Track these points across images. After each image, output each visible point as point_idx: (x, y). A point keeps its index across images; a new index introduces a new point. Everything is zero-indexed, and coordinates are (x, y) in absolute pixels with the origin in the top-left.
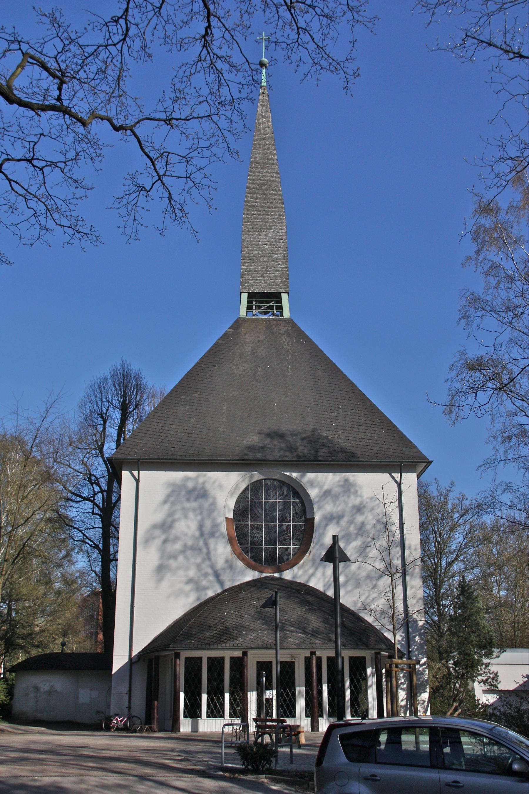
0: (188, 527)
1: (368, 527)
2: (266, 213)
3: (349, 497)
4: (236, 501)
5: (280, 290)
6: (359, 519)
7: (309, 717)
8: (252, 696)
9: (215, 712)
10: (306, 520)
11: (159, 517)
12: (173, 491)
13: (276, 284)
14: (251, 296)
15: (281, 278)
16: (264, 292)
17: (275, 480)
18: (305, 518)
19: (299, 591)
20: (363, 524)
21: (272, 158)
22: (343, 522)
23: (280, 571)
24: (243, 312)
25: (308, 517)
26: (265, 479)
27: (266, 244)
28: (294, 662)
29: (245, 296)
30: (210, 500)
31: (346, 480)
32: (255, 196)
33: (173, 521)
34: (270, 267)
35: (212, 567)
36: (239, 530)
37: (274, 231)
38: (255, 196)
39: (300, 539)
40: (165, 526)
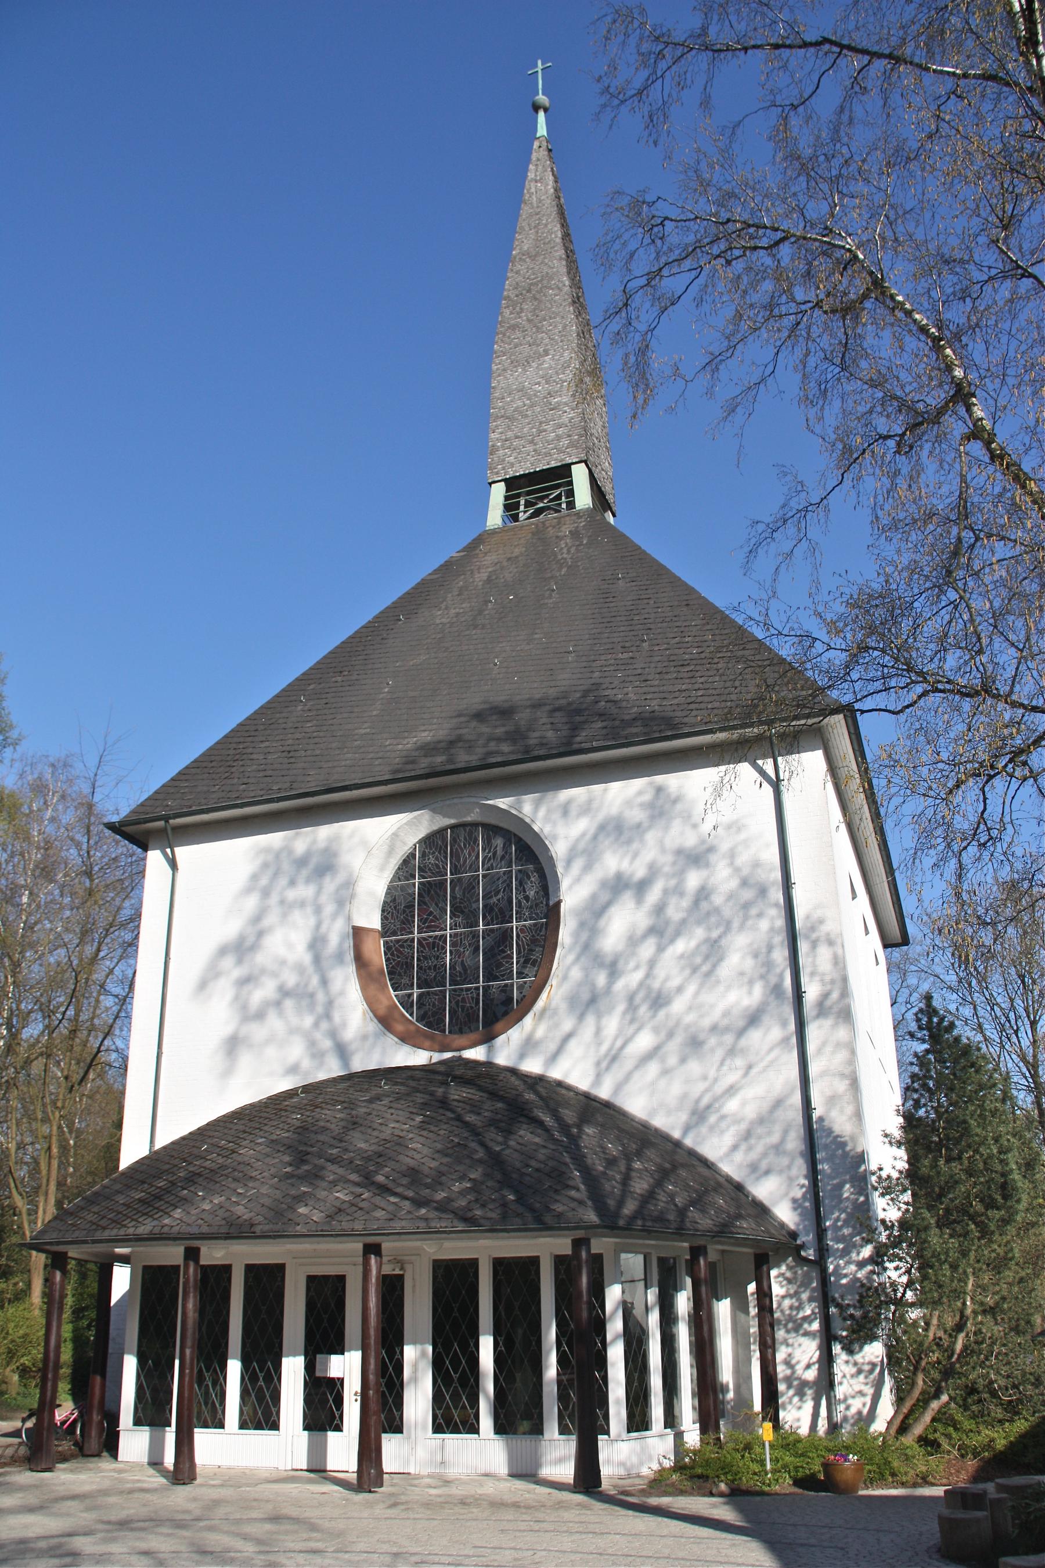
0: (290, 946)
1: (718, 900)
2: (539, 330)
3: (667, 828)
5: (568, 461)
6: (693, 880)
7: (570, 1433)
8: (293, 1370)
9: (262, 1415)
11: (231, 929)
12: (265, 865)
13: (560, 451)
14: (511, 483)
15: (569, 436)
16: (535, 472)
20: (703, 893)
21: (552, 239)
22: (654, 895)
23: (488, 1038)
24: (495, 517)
26: (453, 827)
27: (539, 383)
28: (401, 1277)
29: (498, 492)
30: (341, 878)
31: (659, 790)
32: (518, 309)
33: (260, 934)
34: (547, 423)
35: (333, 1034)
37: (554, 356)
38: (518, 309)
40: (241, 948)
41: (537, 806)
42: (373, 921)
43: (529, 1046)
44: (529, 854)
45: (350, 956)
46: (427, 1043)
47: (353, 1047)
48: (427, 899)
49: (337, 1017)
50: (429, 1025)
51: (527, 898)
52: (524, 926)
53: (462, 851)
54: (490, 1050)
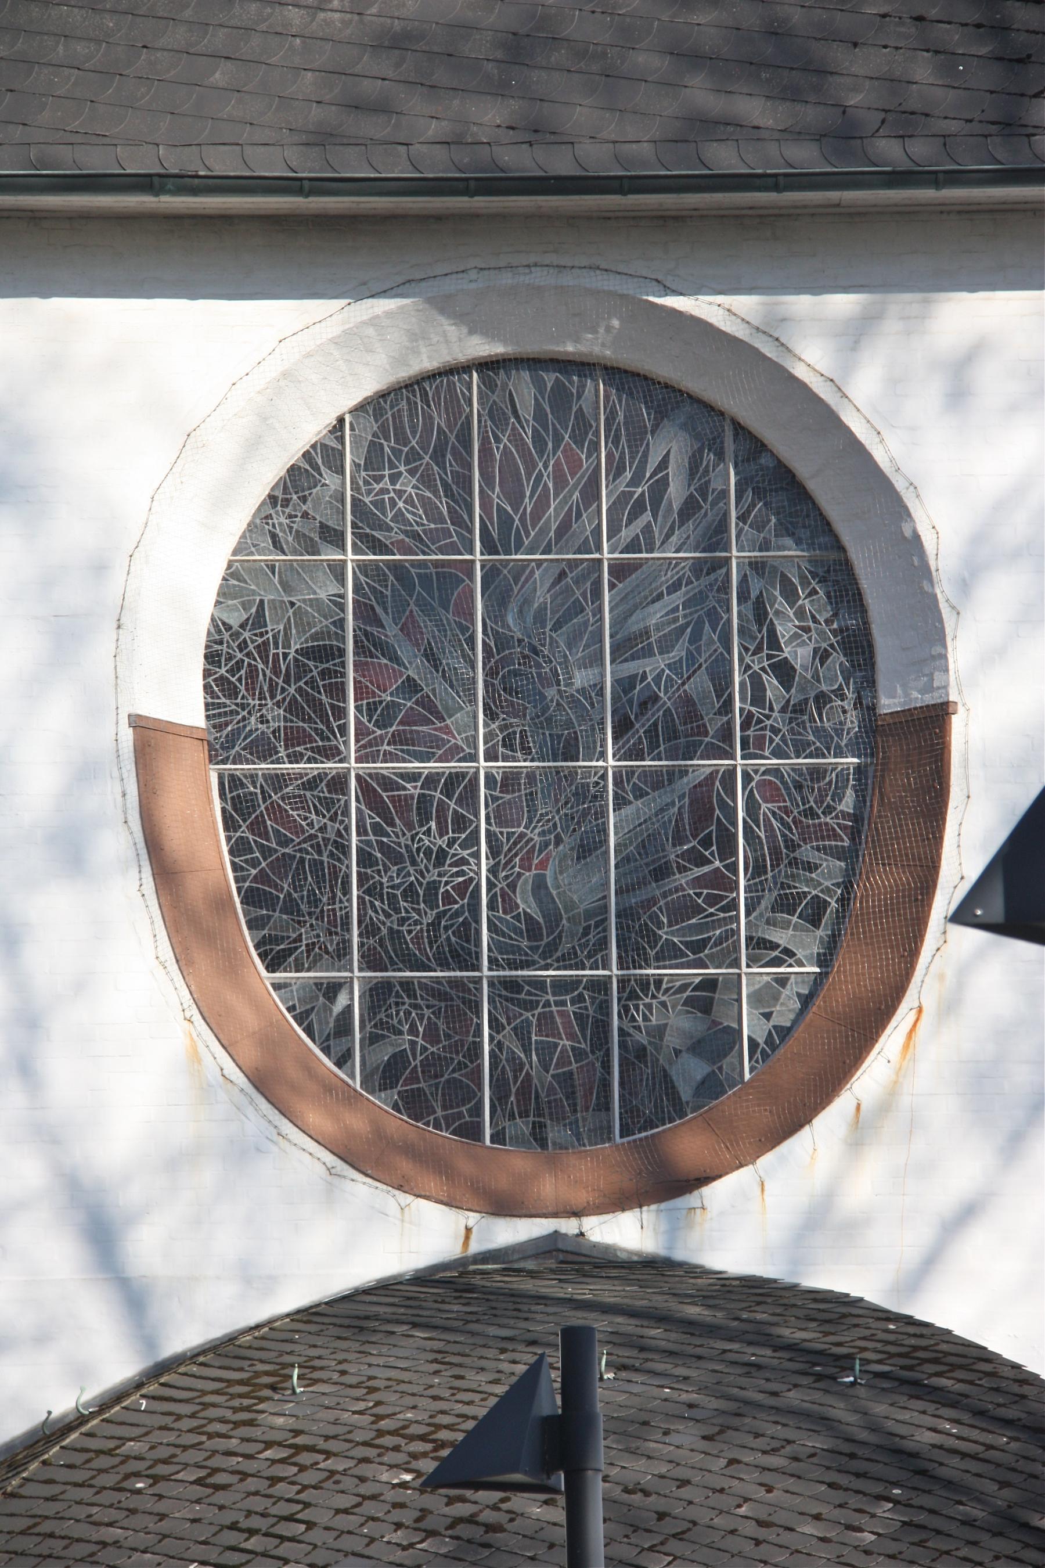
4: (232, 573)
10: (875, 731)
17: (583, 367)
18: (868, 709)
19: (823, 1367)
23: (669, 1184)
25: (888, 704)
26: (487, 366)
36: (258, 827)
39: (818, 908)
41: (855, 336)
42: (186, 704)
43: (819, 1220)
44: (810, 518)
45: (118, 843)
46: (432, 1184)
47: (131, 1196)
48: (391, 632)
49: (61, 1069)
50: (414, 1105)
51: (784, 671)
52: (776, 771)
53: (530, 466)
54: (673, 1232)
